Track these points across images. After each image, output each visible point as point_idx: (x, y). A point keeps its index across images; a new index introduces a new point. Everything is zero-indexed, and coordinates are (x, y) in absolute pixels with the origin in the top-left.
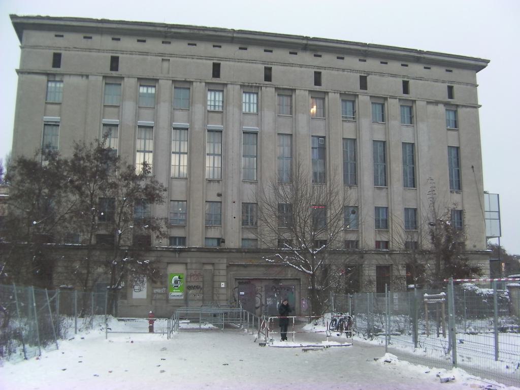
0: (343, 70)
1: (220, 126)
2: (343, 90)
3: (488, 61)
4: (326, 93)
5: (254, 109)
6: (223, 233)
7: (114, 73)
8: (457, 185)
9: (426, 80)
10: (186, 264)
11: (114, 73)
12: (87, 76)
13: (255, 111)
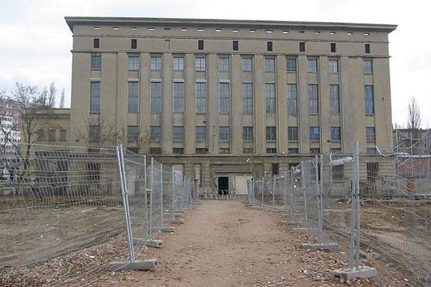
5: (181, 68)
7: (134, 50)
8: (371, 112)
10: (184, 164)
11: (134, 50)
12: (117, 53)
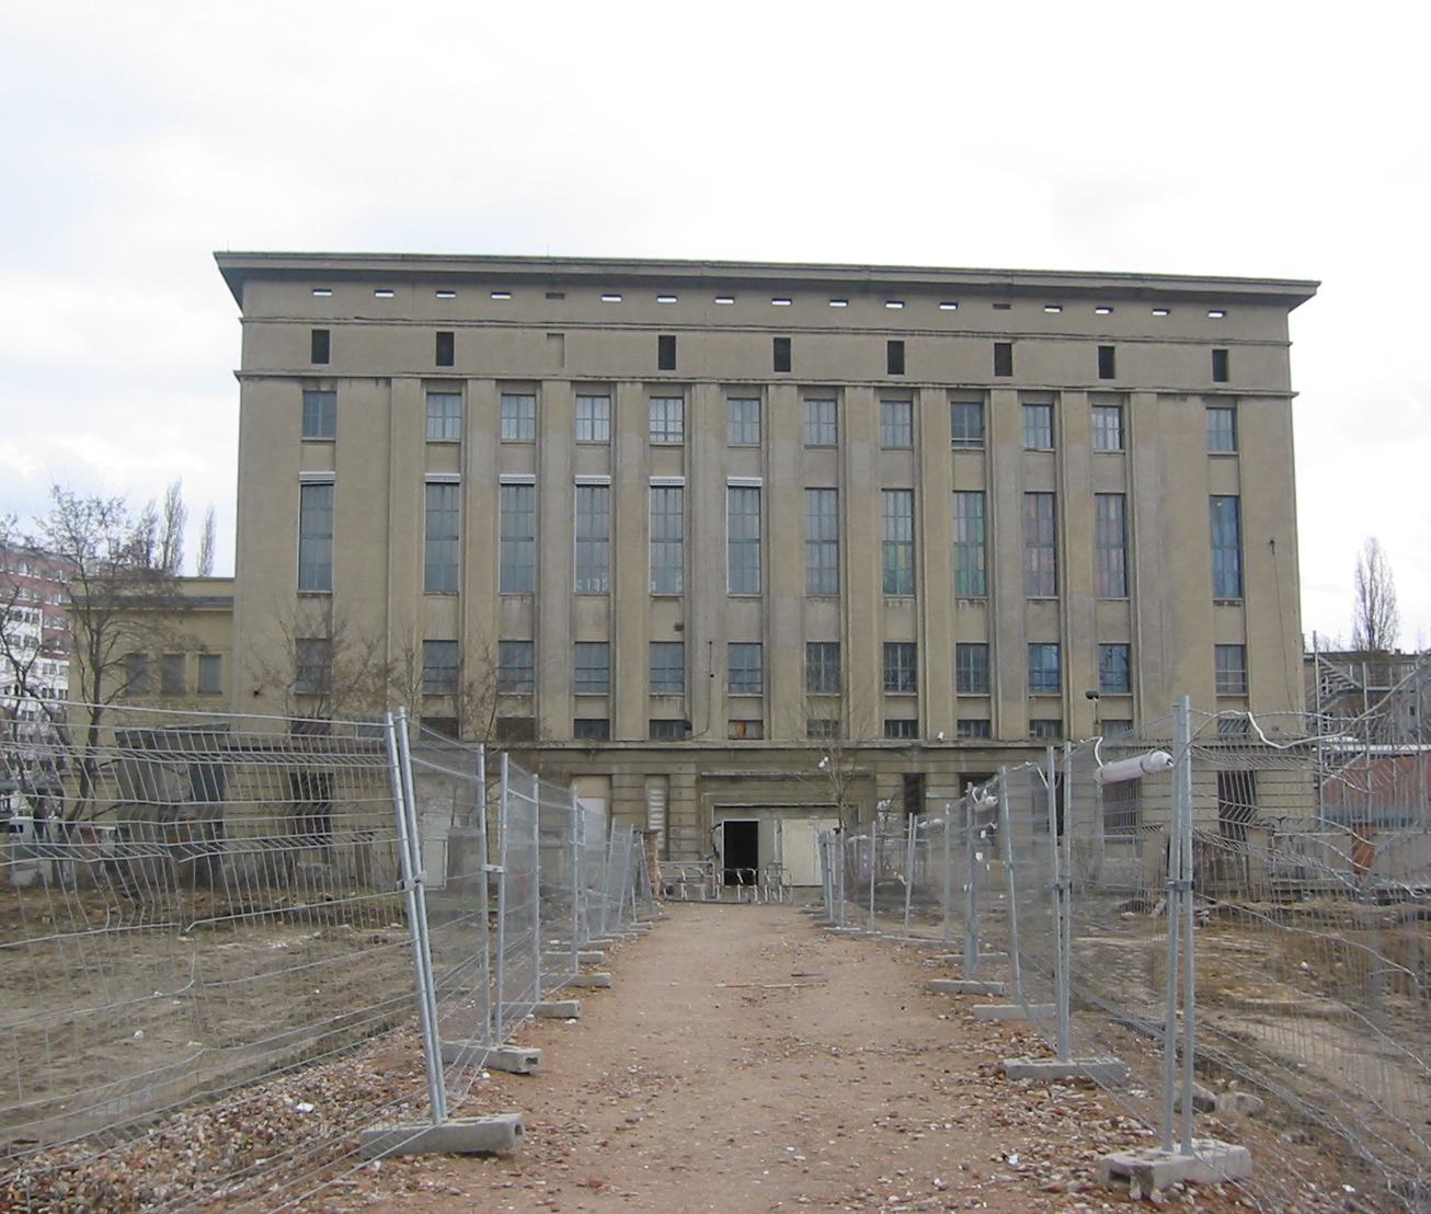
0: (956, 334)
1: (454, 475)
2: (954, 379)
3: (1313, 286)
4: (914, 390)
5: (602, 434)
6: (687, 710)
7: (445, 372)
9: (1157, 342)
10: (610, 776)
13: (606, 438)
